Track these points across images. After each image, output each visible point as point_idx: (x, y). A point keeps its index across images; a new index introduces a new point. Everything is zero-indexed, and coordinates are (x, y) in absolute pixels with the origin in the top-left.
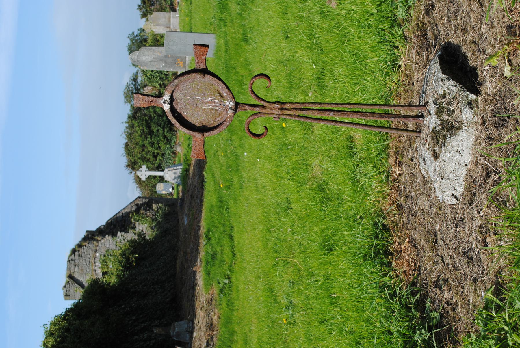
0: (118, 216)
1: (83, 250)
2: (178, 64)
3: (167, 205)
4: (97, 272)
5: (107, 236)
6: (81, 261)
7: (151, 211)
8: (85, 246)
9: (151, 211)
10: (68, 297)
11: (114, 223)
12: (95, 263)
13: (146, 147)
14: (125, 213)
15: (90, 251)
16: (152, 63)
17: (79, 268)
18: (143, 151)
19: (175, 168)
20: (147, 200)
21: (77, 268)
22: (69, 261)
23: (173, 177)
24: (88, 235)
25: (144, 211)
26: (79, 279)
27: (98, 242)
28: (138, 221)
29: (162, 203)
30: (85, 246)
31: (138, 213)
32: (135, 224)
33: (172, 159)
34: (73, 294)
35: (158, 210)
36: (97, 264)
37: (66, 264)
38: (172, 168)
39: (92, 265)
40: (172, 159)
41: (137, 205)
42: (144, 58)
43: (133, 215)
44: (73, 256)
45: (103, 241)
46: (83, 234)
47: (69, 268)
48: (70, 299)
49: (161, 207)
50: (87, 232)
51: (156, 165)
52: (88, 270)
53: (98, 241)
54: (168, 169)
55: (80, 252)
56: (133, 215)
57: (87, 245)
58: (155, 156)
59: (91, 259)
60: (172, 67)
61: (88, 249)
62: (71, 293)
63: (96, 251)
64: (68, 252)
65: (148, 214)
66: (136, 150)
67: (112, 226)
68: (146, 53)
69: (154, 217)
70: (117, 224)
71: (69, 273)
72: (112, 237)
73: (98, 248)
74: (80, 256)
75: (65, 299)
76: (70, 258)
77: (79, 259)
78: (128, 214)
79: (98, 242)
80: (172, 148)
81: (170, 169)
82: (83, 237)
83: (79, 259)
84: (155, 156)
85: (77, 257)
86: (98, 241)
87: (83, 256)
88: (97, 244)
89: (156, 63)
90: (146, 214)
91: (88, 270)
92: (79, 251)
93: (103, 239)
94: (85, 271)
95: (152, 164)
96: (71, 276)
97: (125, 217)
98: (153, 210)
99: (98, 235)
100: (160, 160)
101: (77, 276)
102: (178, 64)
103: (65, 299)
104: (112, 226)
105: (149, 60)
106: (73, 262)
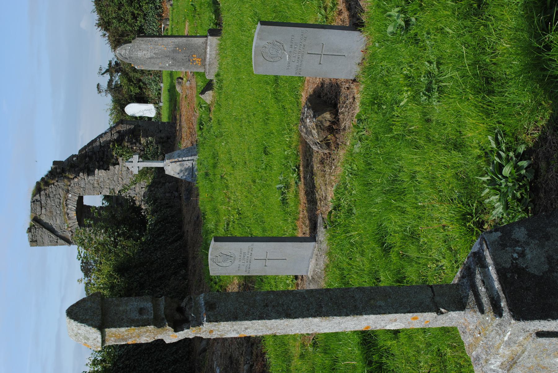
0: (94, 145)
1: (51, 189)
2: (194, 61)
3: (160, 143)
4: (69, 215)
5: (81, 174)
6: (49, 202)
7: (138, 145)
8: (53, 184)
9: (138, 145)
10: (34, 244)
11: (90, 153)
12: (66, 206)
13: (123, 5)
14: (104, 142)
15: (61, 190)
16: (152, 60)
17: (46, 210)
18: (119, 9)
19: (180, 159)
20: (133, 126)
21: (43, 210)
22: (34, 202)
23: (178, 171)
24: (56, 168)
25: (129, 144)
26: (47, 222)
27: (70, 181)
28: (121, 156)
29: (152, 136)
30: (53, 184)
31: (120, 145)
32: (117, 159)
33: (157, 21)
34: (41, 240)
35: (147, 145)
36: (70, 206)
37: (30, 204)
38: (176, 160)
39: (64, 208)
40: (157, 21)
41: (119, 132)
42: (140, 54)
43: (114, 145)
44: (38, 196)
45: (76, 180)
46: (48, 167)
47: (33, 210)
48: (37, 245)
49: (151, 142)
50: (55, 163)
51: (137, 28)
52: (58, 212)
53: (69, 179)
54: (171, 160)
55: (47, 192)
56: (114, 145)
57: (56, 184)
58: (135, 17)
59: (62, 199)
60: (183, 65)
61: (57, 188)
62: (39, 238)
63: (68, 191)
64: (32, 186)
65: (135, 148)
66: (110, 9)
67: (87, 159)
68: (143, 46)
69: (142, 153)
70: (94, 156)
71: (35, 215)
72: (88, 175)
73: (70, 188)
74: (48, 196)
75: (31, 246)
76: (35, 198)
77: (46, 200)
78: (108, 143)
79: (70, 181)
80: (156, 9)
81: (173, 160)
82: (50, 169)
83: (46, 200)
84: (135, 17)
85: (43, 198)
86: (69, 179)
87: (51, 196)
88: (69, 184)
89: (158, 61)
90: (132, 148)
91: (58, 212)
92: (45, 190)
93: (76, 177)
94: (55, 213)
95: (131, 26)
96: (36, 220)
97: (103, 147)
98: (140, 144)
99: (69, 171)
100: (140, 22)
101: (44, 219)
102: (194, 61)
103: (31, 246)
104: (87, 159)
105: (149, 55)
106: (38, 203)
